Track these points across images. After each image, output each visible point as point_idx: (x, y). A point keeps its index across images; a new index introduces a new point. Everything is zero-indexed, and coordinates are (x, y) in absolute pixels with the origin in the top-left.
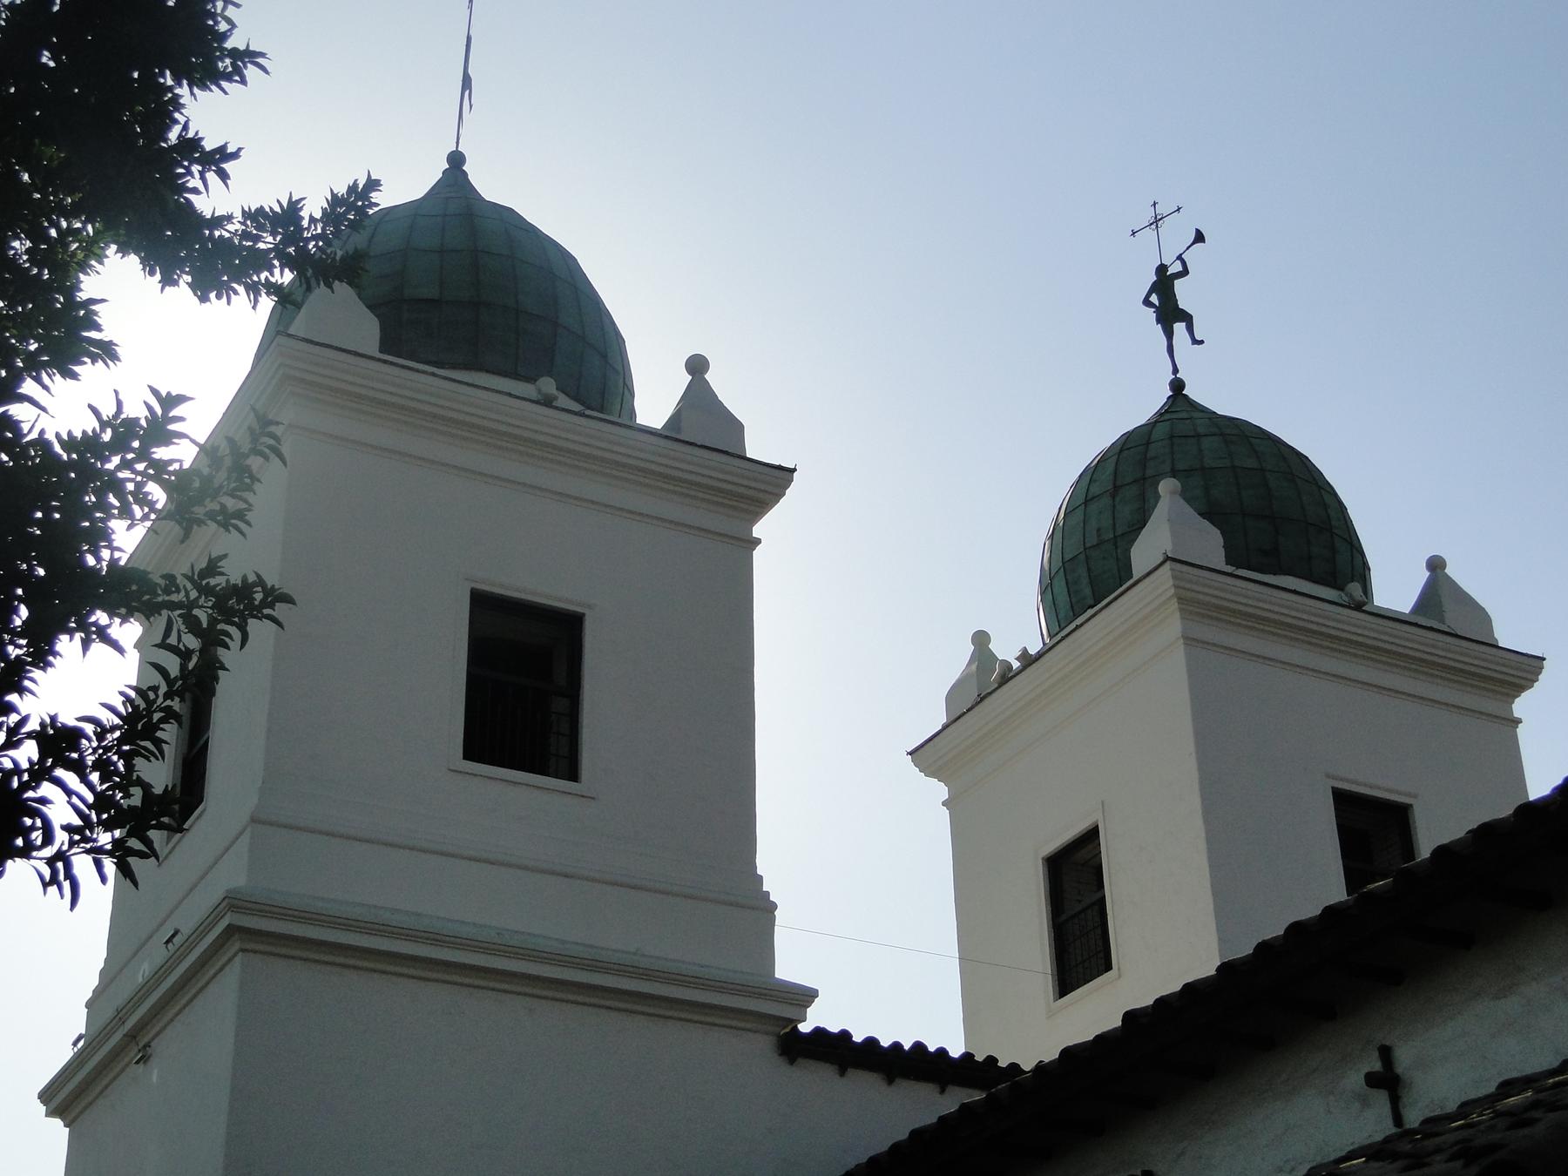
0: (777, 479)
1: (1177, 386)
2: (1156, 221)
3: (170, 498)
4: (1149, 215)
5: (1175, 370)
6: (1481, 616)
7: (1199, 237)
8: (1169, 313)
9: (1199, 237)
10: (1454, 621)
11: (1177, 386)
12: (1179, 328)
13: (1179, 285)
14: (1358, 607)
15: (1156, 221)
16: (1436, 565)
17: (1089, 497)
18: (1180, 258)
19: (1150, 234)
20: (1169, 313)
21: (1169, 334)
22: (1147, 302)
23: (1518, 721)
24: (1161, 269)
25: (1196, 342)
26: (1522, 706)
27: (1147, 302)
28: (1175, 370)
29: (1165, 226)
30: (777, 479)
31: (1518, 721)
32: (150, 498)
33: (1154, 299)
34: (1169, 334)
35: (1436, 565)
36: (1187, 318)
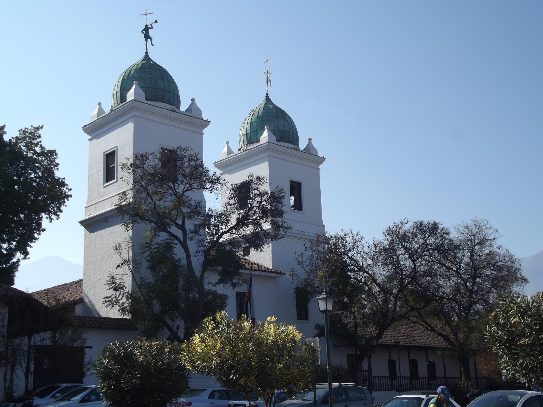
0: (207, 123)
1: (147, 53)
2: (147, 14)
3: (34, 236)
4: (145, 12)
5: (147, 50)
6: (316, 150)
7: (156, 21)
8: (147, 37)
9: (156, 21)
10: (312, 152)
11: (147, 53)
12: (149, 40)
13: (150, 30)
14: (297, 150)
15: (147, 14)
16: (193, 100)
17: (129, 78)
18: (151, 24)
19: (145, 16)
20: (147, 37)
21: (146, 41)
22: (142, 32)
23: (320, 169)
24: (147, 26)
25: (152, 45)
26: (321, 166)
27: (142, 32)
28: (147, 50)
29: (149, 15)
30: (207, 123)
31: (320, 169)
32: (225, 304)
33: (144, 32)
34: (146, 41)
35: (193, 100)
36: (151, 39)
